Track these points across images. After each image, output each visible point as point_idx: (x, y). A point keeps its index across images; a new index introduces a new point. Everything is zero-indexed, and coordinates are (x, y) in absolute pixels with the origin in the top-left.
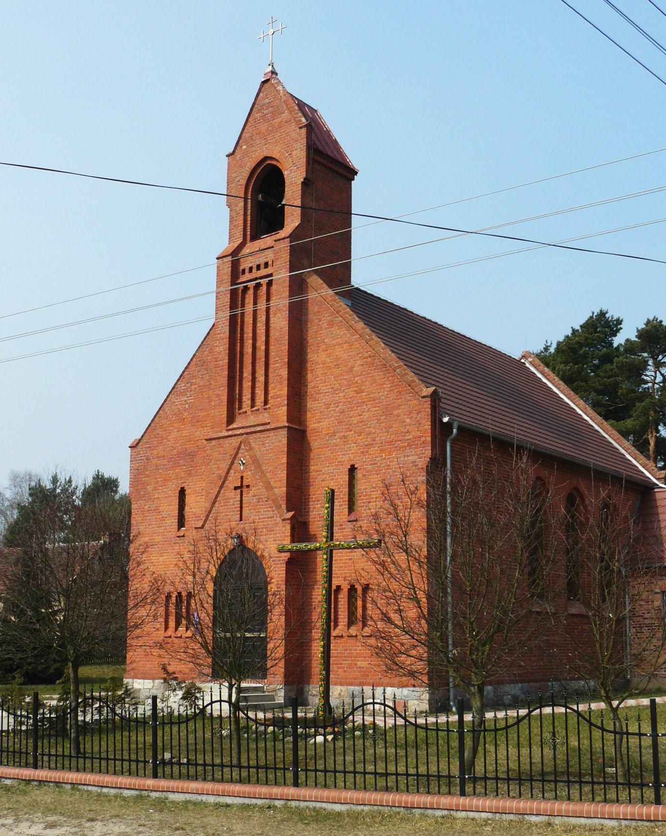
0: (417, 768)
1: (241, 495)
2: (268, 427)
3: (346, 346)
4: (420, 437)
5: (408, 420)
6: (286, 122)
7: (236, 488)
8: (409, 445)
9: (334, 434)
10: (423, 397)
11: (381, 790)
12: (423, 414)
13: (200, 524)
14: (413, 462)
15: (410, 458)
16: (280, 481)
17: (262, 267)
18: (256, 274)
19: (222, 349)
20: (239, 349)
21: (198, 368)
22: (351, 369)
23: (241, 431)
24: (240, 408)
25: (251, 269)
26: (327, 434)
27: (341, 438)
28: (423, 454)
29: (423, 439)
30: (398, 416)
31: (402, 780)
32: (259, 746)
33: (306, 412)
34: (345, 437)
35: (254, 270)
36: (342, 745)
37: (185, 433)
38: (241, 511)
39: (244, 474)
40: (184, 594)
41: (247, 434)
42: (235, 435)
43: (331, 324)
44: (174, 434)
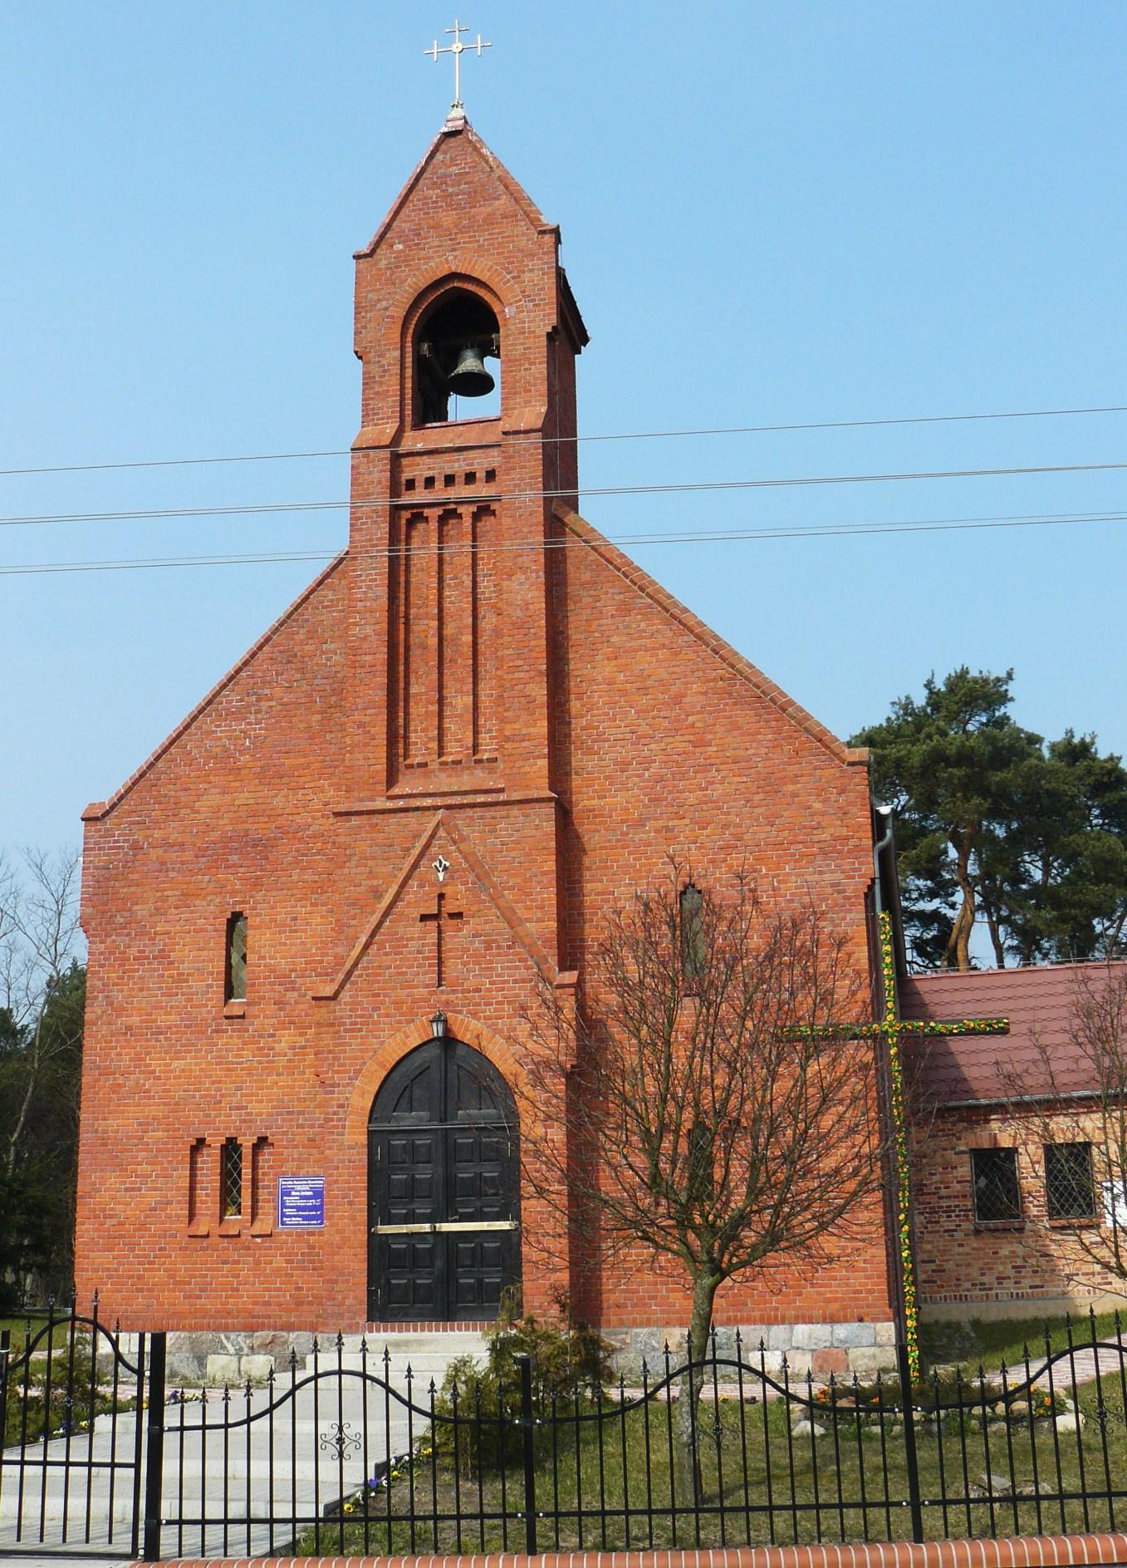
0: (1036, 1483)
1: (440, 932)
2: (502, 797)
3: (661, 654)
4: (847, 838)
5: (818, 806)
6: (504, 216)
7: (424, 918)
8: (825, 853)
9: (640, 823)
10: (852, 764)
11: (982, 1536)
12: (852, 796)
13: (328, 991)
14: (832, 885)
15: (826, 876)
16: (541, 908)
17: (460, 479)
18: (440, 493)
19: (369, 630)
20: (402, 636)
21: (280, 668)
22: (678, 700)
23: (428, 802)
24: (406, 757)
25: (430, 482)
26: (623, 822)
27: (657, 831)
28: (855, 870)
29: (852, 842)
30: (795, 795)
31: (448, 1530)
32: (947, 1455)
33: (568, 774)
34: (668, 829)
35: (439, 484)
36: (797, 1453)
37: (242, 798)
38: (440, 964)
39: (448, 890)
40: (247, 1142)
41: (448, 807)
42: (417, 809)
43: (624, 609)
44: (213, 799)
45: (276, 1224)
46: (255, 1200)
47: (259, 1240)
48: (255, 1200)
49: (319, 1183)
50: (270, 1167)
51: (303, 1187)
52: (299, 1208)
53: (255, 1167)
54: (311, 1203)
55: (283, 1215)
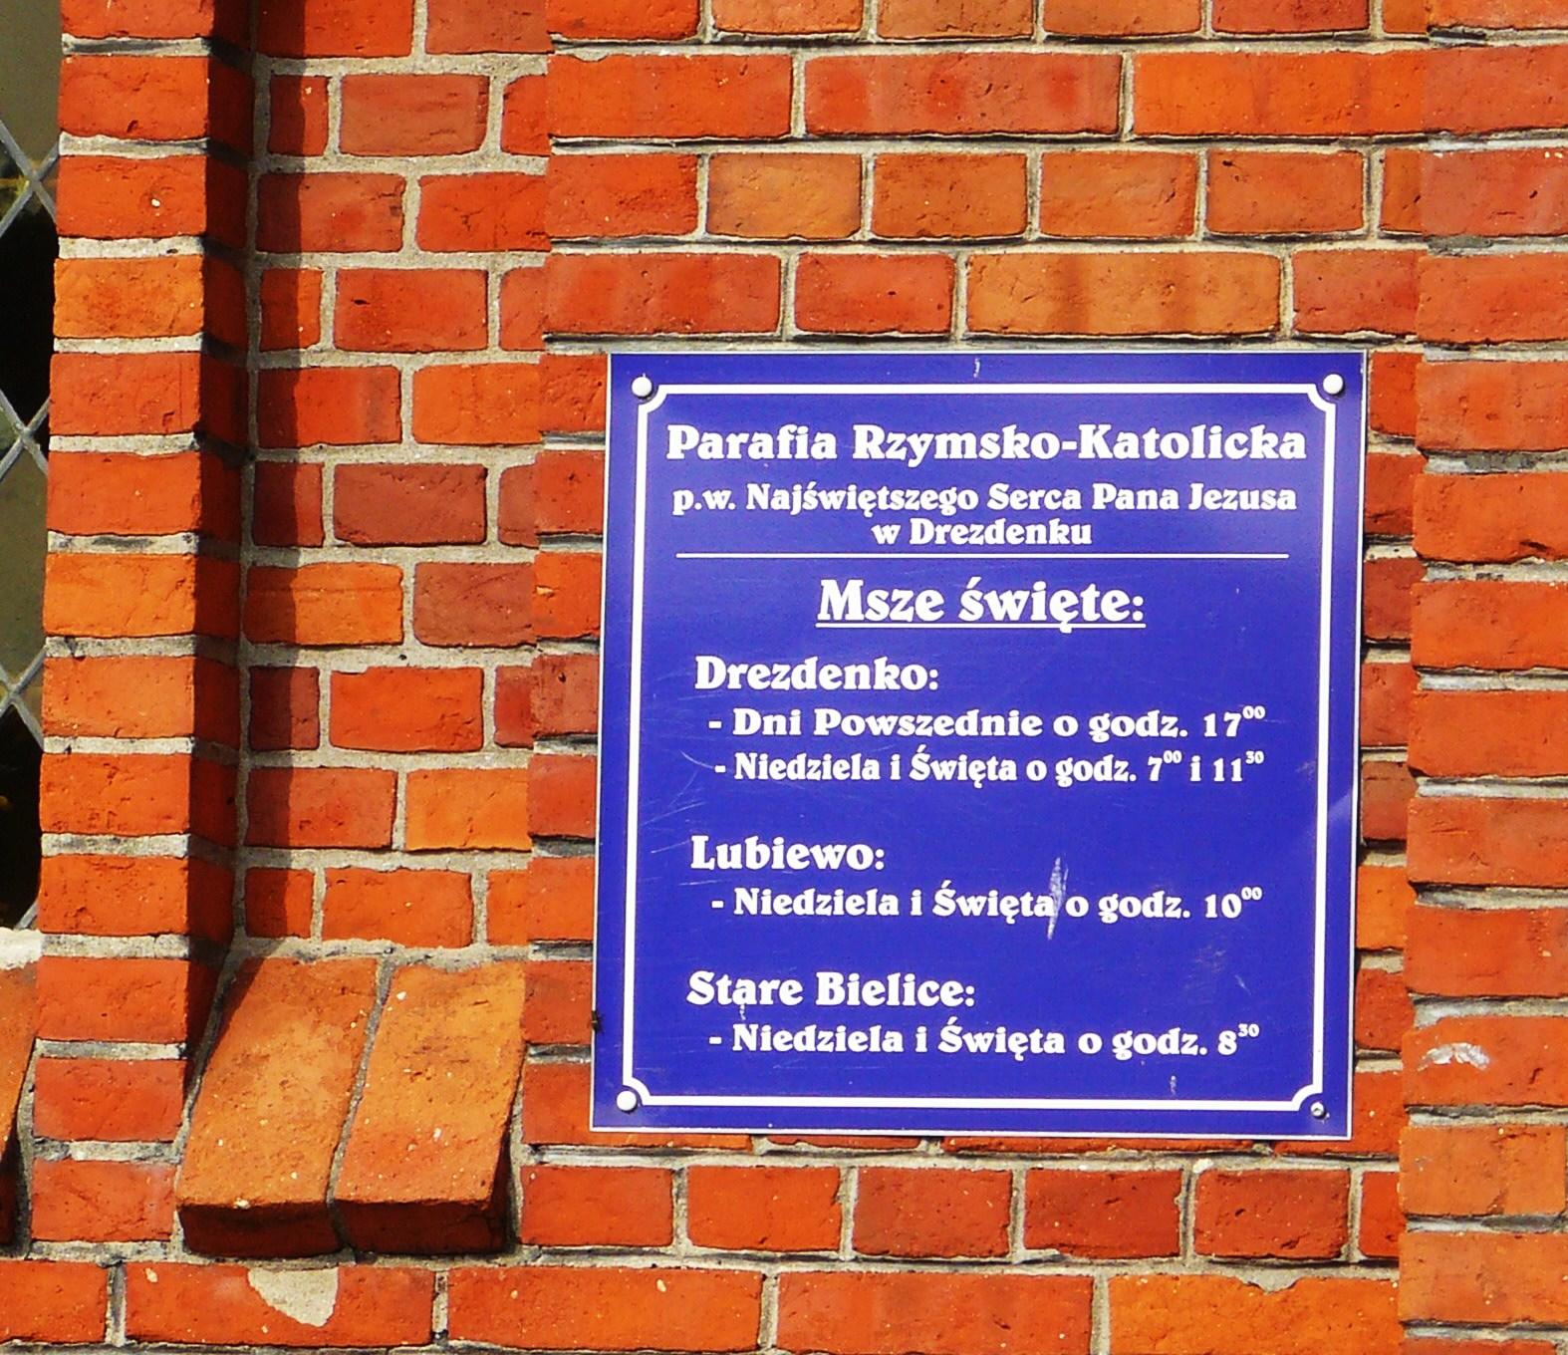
45: (566, 1051)
46: (244, 703)
47: (302, 1294)
48: (244, 703)
49: (1277, 473)
50: (460, 215)
51: (991, 519)
52: (924, 831)
53: (250, 208)
54: (1108, 749)
55: (692, 924)
